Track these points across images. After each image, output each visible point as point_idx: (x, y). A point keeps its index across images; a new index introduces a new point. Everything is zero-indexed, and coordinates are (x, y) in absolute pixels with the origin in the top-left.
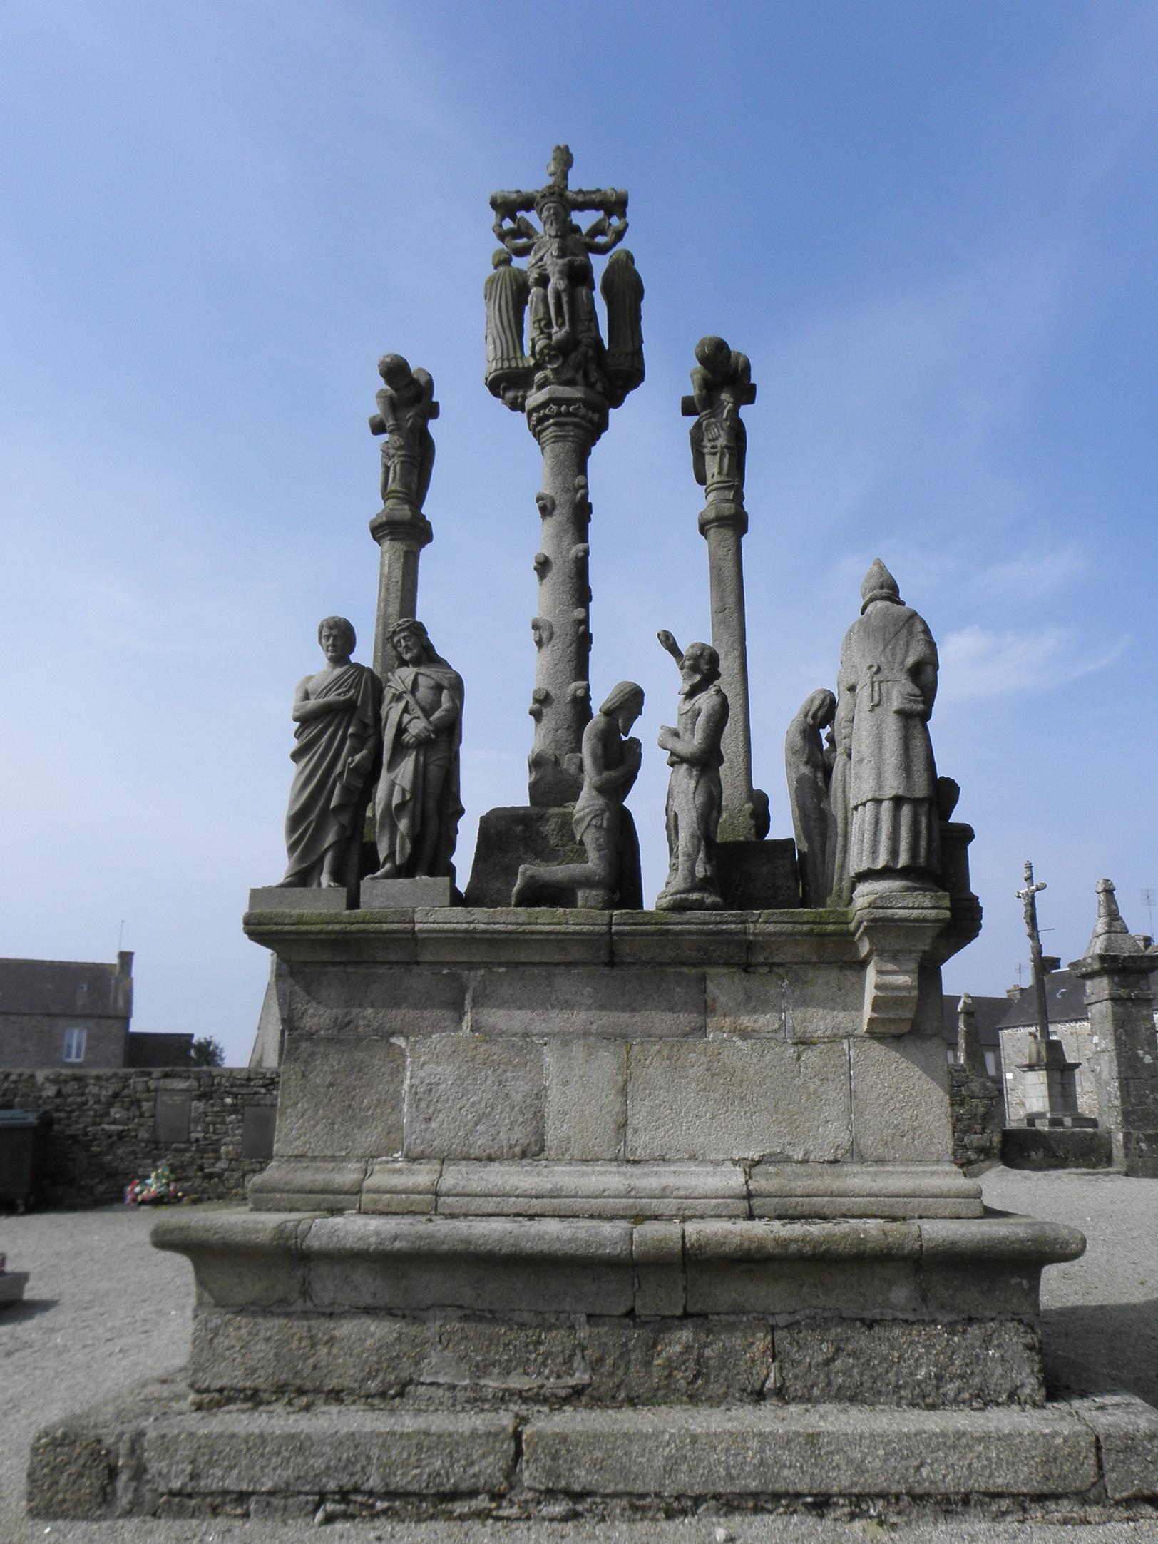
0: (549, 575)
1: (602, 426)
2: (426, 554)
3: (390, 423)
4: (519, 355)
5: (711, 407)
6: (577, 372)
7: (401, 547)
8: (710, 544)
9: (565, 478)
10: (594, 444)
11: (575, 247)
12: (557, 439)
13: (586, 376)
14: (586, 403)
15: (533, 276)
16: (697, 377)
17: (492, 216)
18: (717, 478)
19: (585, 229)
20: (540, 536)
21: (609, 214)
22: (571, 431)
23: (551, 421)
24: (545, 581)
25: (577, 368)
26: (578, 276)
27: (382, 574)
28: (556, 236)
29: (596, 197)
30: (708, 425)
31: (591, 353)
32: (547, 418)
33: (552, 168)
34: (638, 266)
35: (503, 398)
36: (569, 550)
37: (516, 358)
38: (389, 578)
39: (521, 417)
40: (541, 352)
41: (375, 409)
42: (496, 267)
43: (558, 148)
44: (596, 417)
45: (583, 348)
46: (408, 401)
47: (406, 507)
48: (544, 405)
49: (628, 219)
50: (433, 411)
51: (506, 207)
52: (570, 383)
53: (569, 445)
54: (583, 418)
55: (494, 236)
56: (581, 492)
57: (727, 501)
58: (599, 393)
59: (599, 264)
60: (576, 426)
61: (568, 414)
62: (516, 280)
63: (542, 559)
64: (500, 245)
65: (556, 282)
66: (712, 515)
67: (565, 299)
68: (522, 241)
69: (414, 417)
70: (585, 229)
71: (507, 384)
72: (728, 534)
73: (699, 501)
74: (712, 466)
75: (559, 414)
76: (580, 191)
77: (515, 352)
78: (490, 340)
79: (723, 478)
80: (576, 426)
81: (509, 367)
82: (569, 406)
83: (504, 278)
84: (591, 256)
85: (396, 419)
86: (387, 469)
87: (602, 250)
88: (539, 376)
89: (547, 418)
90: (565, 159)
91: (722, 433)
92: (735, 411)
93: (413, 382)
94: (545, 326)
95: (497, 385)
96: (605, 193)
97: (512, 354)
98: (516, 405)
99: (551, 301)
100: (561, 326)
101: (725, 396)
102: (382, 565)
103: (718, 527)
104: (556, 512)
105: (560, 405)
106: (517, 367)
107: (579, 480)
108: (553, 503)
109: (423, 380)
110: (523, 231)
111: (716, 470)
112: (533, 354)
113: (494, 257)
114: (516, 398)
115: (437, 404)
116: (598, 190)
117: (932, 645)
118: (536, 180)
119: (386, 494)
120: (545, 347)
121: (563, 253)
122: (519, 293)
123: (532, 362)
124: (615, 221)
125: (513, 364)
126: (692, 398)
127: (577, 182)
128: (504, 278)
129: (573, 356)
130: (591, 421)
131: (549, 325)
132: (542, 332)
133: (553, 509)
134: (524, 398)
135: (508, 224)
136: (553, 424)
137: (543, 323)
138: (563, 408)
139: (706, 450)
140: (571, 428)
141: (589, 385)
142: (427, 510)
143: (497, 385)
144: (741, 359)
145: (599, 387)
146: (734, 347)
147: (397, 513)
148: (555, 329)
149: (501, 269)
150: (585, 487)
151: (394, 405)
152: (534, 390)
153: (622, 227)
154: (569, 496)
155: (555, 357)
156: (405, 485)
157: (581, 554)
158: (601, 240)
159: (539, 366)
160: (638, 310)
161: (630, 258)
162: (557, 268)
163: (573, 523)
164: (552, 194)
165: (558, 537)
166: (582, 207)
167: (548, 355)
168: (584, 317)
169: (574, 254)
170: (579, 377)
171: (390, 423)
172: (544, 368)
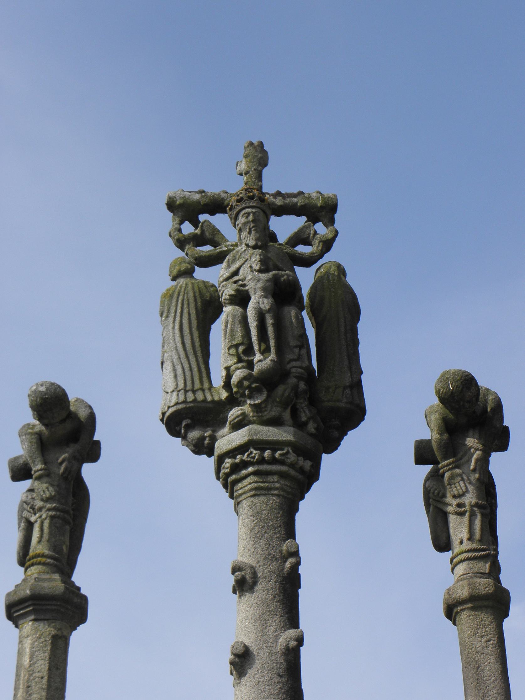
0: (251, 672)
1: (311, 476)
2: (79, 638)
3: (37, 467)
4: (206, 385)
5: (454, 456)
6: (285, 409)
7: (47, 630)
8: (461, 632)
9: (269, 544)
10: (302, 498)
11: (279, 260)
12: (258, 492)
13: (295, 413)
14: (297, 449)
15: (227, 291)
16: (435, 418)
17: (168, 220)
18: (467, 545)
19: (282, 238)
20: (237, 620)
21: (313, 219)
22: (275, 482)
23: (251, 469)
24: (244, 680)
25: (284, 404)
26: (284, 293)
27: (19, 666)
28: (255, 247)
29: (299, 201)
30: (452, 477)
31: (302, 386)
32: (245, 464)
33: (243, 166)
34: (351, 280)
35: (184, 438)
36: (277, 638)
37: (203, 390)
38: (31, 672)
39: (209, 463)
40: (240, 384)
41: (18, 449)
42: (174, 279)
43: (251, 144)
44: (307, 465)
45: (292, 381)
46: (63, 434)
47: (57, 576)
48: (241, 449)
49: (337, 226)
50: (93, 452)
51: (185, 209)
52: (275, 422)
53: (274, 500)
54: (292, 466)
55: (171, 243)
56: (291, 560)
57: (482, 575)
58: (311, 435)
59: (306, 277)
60: (282, 475)
61: (273, 461)
62: (201, 295)
63: (240, 650)
64: (180, 254)
65: (257, 301)
66: (464, 593)
67: (270, 321)
68: (207, 249)
69: (68, 460)
70: (282, 238)
71: (191, 421)
72: (486, 618)
73: (442, 575)
74: (459, 529)
75: (262, 461)
76: (279, 194)
77: (202, 382)
78: (168, 366)
79: (475, 546)
80: (282, 475)
81: (195, 401)
82: (274, 450)
83: (186, 292)
84: (297, 269)
85: (45, 463)
86: (29, 526)
87: (307, 262)
88: (234, 413)
89: (245, 464)
90: (259, 157)
91: (470, 488)
92: (484, 462)
93: (71, 416)
94: (243, 352)
95: (176, 423)
96: (309, 197)
97: (197, 385)
98: (202, 448)
99: (253, 323)
100: (265, 351)
101: (471, 442)
102: (20, 653)
103: (472, 609)
104: (259, 587)
105: (263, 450)
106: (205, 401)
107: (286, 546)
108: (255, 574)
109: (83, 414)
110: (209, 237)
111: (465, 535)
112: (227, 385)
113: (172, 266)
114: (203, 438)
115: (98, 443)
116: (301, 193)
117: (90, 407)
118: (229, 182)
119: (24, 559)
120: (245, 378)
121: (265, 268)
122: (208, 307)
123: (224, 395)
124: (320, 228)
125: (200, 396)
126: (429, 442)
127: (276, 181)
128: (186, 292)
129: (280, 389)
130: (301, 470)
131: (249, 351)
132: (240, 360)
133: (255, 583)
134: (213, 439)
135: (188, 229)
136: (254, 473)
137: (241, 349)
138: (267, 453)
139: (450, 509)
140: (276, 478)
141: (299, 425)
142: (78, 577)
143: (176, 423)
144: (491, 397)
145: (311, 427)
146: (482, 382)
147: (46, 585)
148: (258, 357)
149: (182, 281)
150: (296, 554)
151: (43, 445)
152: (226, 429)
153: (331, 236)
154: (275, 566)
155: (258, 391)
156: (55, 547)
157: (293, 644)
158: (302, 249)
159: (233, 401)
160: (355, 332)
161: (341, 271)
162: (260, 284)
163: (282, 602)
164: (251, 198)
165: (261, 621)
166: (280, 211)
167: (249, 387)
168: (293, 343)
169: (277, 268)
170: (287, 415)
171: (37, 467)
172: (239, 404)
